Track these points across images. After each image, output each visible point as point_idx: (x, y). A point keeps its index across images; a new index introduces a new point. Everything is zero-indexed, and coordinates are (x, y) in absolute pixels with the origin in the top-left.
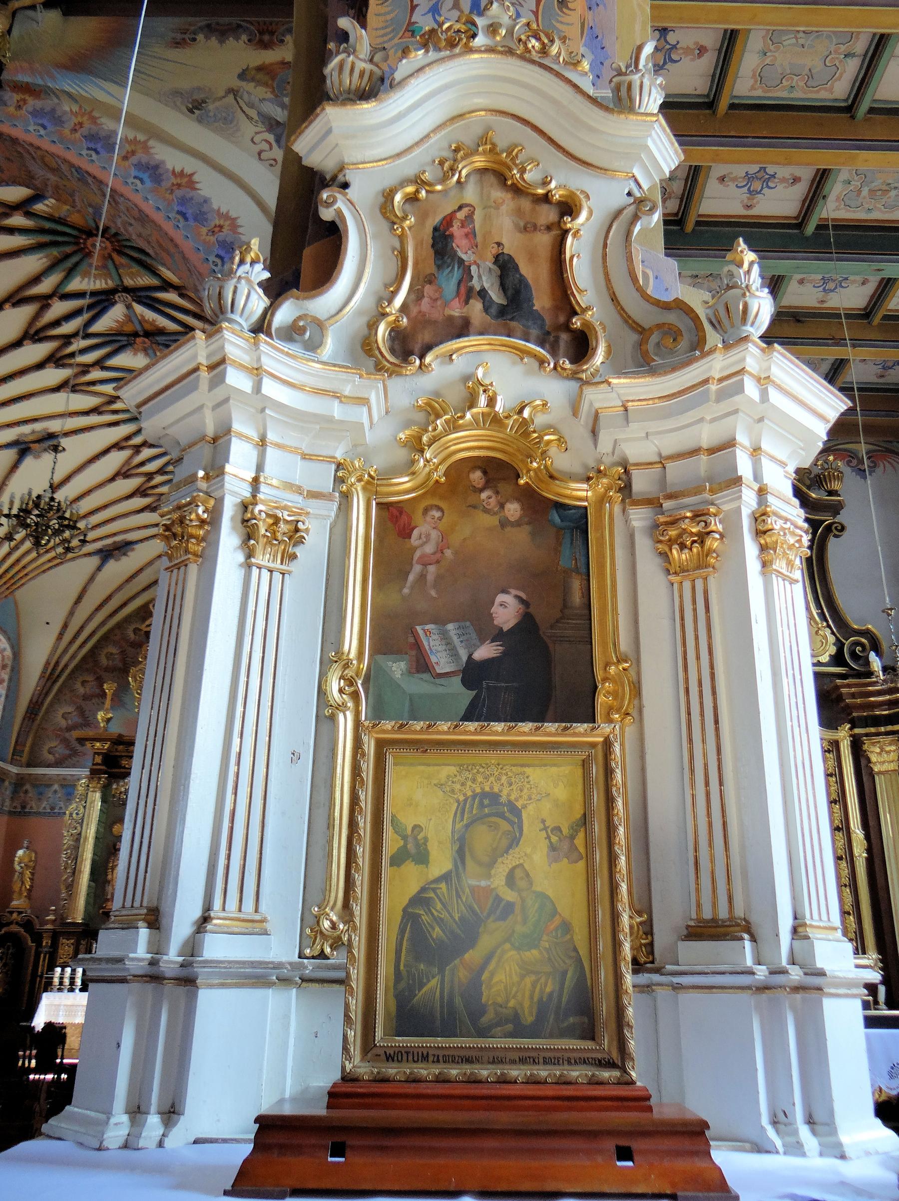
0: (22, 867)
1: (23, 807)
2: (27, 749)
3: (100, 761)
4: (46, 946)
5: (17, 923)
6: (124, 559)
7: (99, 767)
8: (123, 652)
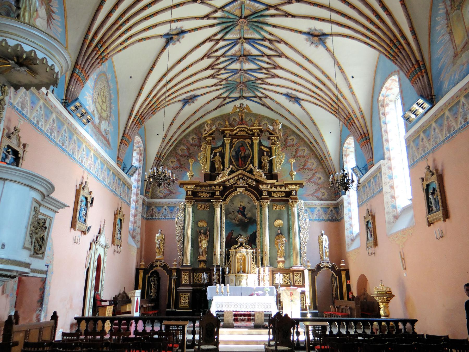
1: (152, 216)
2: (150, 191)
3: (190, 194)
4: (174, 276)
6: (192, 104)
7: (190, 196)
8: (188, 148)
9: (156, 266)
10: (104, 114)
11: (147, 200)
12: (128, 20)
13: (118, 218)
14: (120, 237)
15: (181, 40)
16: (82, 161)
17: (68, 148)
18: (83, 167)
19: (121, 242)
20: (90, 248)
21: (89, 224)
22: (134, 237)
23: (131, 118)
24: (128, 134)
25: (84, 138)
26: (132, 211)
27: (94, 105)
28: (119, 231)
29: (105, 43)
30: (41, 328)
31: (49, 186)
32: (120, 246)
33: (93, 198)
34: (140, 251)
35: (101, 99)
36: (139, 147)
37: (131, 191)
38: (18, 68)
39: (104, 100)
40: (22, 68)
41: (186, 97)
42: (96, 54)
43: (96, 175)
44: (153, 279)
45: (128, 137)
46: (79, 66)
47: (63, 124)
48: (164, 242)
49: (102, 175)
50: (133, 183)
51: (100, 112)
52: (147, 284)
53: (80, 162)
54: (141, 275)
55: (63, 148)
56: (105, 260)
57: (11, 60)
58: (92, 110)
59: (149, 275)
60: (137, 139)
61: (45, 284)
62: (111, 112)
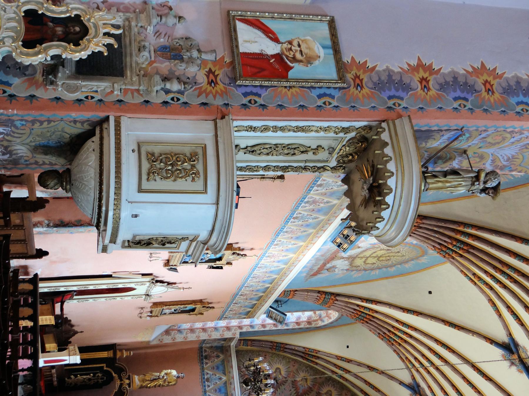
0: (163, 377)
1: (206, 358)
2: (249, 347)
5: (121, 385)
9: (121, 379)
10: (359, 262)
11: (233, 344)
12: (515, 282)
13: (196, 306)
14: (165, 314)
15: (514, 368)
16: (277, 245)
17: (292, 225)
18: (269, 246)
19: (157, 316)
20: (143, 275)
21: (182, 268)
22: (167, 332)
23: (363, 302)
24: (337, 300)
25: (312, 242)
26: (210, 324)
27: (369, 246)
28: (175, 310)
29: (469, 252)
30: (28, 240)
31: (218, 249)
32: (151, 316)
33: (221, 268)
34: (147, 346)
35: (383, 255)
36: (320, 318)
37: (245, 318)
38: (366, 187)
39: (381, 259)
40: (367, 191)
41: (423, 389)
42: (445, 241)
43: (259, 266)
44: (98, 376)
45: (331, 301)
46: (420, 222)
47: (326, 214)
48: (163, 386)
49: (261, 274)
50: (257, 318)
51: (362, 255)
52: (90, 366)
53: (276, 243)
54: (104, 354)
55: (290, 219)
56: (126, 298)
57: (373, 180)
58: (360, 245)
59: (105, 368)
60: (334, 315)
61: (87, 226)
62: (365, 270)
